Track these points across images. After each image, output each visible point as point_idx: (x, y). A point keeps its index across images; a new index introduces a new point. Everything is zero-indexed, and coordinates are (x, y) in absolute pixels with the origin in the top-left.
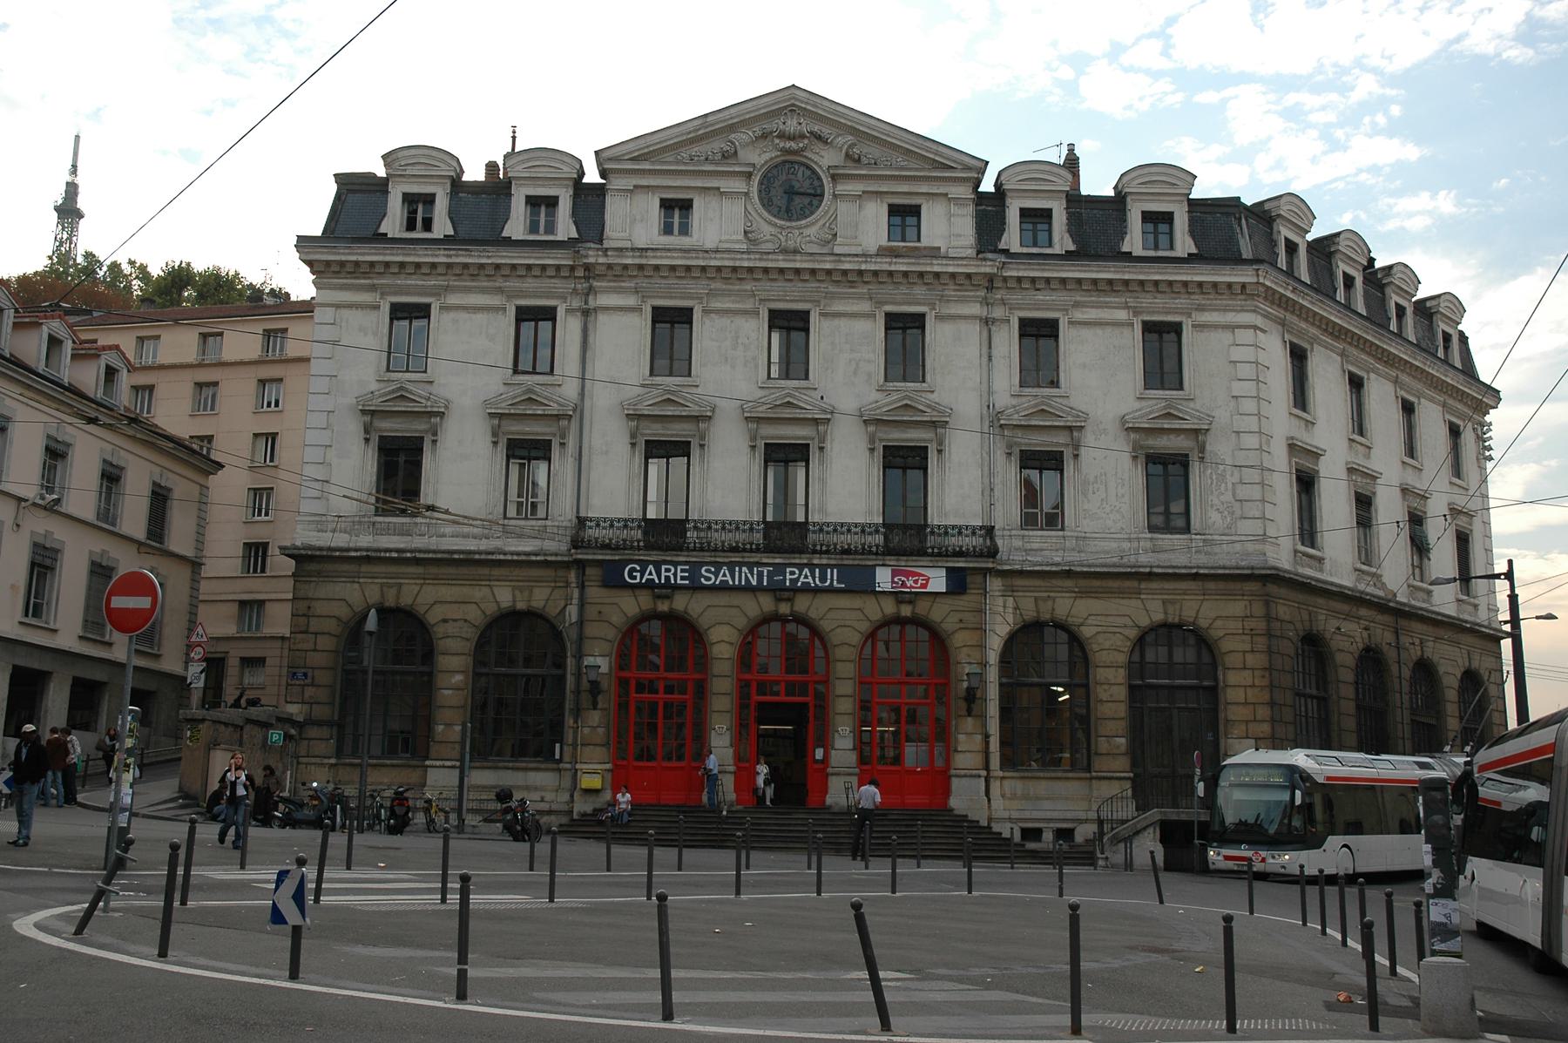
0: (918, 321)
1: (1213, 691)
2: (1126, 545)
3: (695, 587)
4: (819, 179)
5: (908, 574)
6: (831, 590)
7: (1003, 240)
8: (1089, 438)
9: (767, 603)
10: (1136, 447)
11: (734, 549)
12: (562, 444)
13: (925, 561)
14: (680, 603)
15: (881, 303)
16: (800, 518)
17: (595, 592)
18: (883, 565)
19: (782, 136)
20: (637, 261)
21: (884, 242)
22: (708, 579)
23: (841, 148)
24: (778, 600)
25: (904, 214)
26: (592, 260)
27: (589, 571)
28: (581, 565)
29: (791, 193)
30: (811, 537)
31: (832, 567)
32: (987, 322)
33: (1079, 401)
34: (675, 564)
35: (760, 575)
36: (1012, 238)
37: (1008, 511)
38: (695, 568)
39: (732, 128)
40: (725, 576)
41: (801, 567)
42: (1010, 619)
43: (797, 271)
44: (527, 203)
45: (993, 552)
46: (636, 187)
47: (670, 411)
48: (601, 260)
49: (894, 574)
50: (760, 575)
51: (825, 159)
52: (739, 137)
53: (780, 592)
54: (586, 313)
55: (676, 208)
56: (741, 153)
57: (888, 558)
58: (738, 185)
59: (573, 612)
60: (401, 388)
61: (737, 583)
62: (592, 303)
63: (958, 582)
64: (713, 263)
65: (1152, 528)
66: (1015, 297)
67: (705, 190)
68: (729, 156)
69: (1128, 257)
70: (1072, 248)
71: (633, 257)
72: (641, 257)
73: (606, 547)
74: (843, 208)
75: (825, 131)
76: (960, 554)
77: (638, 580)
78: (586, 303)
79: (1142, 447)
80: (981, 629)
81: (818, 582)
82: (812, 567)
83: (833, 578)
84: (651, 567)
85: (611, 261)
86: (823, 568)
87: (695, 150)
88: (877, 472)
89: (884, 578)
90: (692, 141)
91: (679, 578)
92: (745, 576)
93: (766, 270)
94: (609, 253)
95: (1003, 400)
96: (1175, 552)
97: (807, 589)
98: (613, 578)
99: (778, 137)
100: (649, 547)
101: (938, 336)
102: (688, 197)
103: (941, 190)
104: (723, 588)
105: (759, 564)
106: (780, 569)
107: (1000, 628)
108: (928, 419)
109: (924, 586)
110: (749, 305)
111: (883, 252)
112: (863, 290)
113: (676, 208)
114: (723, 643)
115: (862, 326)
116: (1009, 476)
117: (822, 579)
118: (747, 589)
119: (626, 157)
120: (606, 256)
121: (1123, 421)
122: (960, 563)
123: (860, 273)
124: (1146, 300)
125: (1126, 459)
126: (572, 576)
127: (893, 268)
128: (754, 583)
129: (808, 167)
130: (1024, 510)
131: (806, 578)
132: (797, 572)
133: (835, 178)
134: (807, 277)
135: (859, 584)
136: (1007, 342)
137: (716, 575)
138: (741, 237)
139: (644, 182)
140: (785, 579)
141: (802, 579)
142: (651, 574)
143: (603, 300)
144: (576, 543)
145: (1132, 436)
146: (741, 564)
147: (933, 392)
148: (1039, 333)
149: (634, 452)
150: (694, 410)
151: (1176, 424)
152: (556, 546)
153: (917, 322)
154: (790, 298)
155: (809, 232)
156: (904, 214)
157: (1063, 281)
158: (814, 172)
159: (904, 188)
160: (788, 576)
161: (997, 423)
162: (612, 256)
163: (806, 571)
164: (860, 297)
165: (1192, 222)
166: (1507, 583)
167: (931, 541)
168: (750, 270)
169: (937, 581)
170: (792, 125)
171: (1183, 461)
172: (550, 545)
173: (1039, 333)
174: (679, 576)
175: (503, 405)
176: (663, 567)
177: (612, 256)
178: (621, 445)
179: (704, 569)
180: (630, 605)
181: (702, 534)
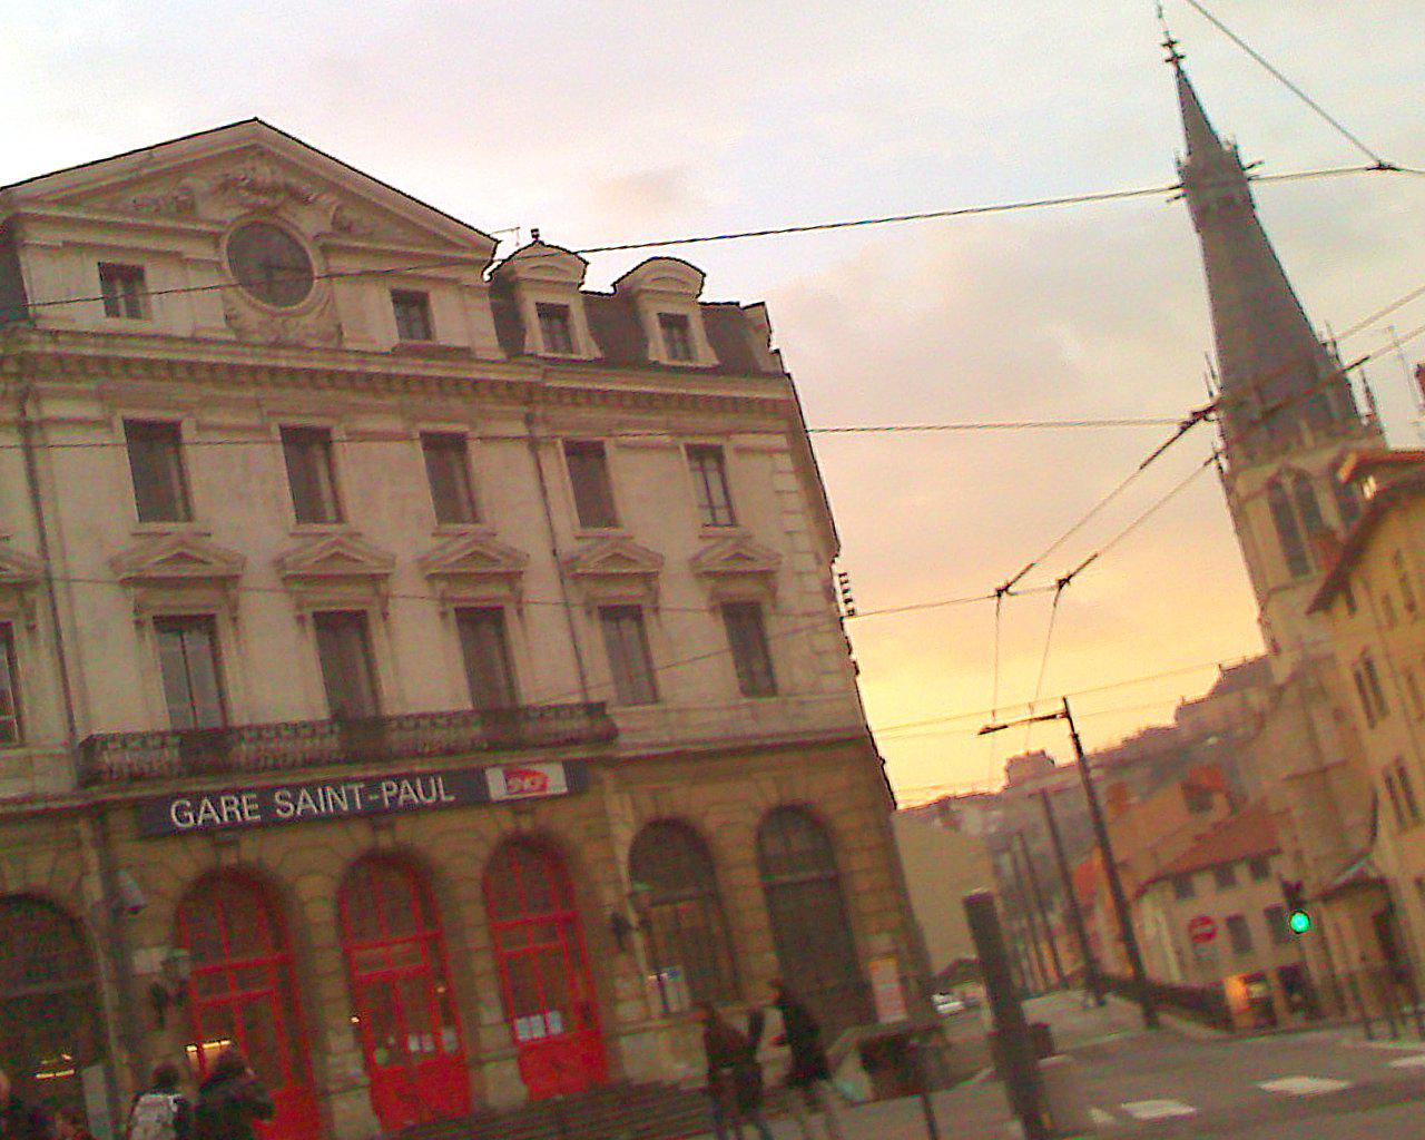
0: (458, 443)
1: (835, 882)
2: (726, 715)
3: (270, 822)
4: (302, 250)
5: (524, 774)
6: (438, 806)
7: (527, 344)
8: (664, 584)
9: (360, 837)
10: (714, 595)
11: (310, 762)
12: (32, 629)
13: (540, 755)
14: (250, 850)
15: (415, 419)
16: (369, 711)
17: (129, 849)
18: (494, 766)
19: (253, 187)
20: (102, 352)
21: (396, 339)
22: (286, 810)
23: (326, 212)
24: (375, 828)
25: (411, 305)
26: (34, 348)
27: (114, 819)
28: (98, 812)
29: (269, 267)
30: (244, 749)
31: (435, 774)
32: (533, 444)
33: (643, 539)
34: (239, 792)
35: (350, 794)
36: (536, 339)
37: (602, 685)
38: (264, 795)
39: (181, 170)
40: (305, 803)
41: (398, 779)
42: (630, 818)
43: (312, 374)
44: (395, 302)
45: (610, 735)
46: (66, 244)
47: (186, 571)
48: (49, 349)
49: (508, 775)
50: (350, 794)
51: (308, 223)
52: (199, 183)
53: (374, 815)
54: (25, 427)
55: (122, 281)
56: (201, 206)
57: (502, 754)
58: (203, 251)
59: (94, 889)
60: (183, 542)
61: (323, 809)
62: (32, 414)
63: (578, 777)
64: (204, 358)
65: (746, 692)
66: (559, 414)
67: (441, 281)
68: (186, 208)
69: (656, 366)
70: (598, 354)
71: (96, 346)
72: (105, 346)
73: (137, 777)
74: (340, 288)
75: (305, 186)
76: (574, 741)
77: (290, 813)
78: (24, 413)
79: (453, 600)
80: (606, 837)
81: (422, 797)
82: (411, 777)
83: (439, 791)
84: (206, 801)
85: (61, 349)
86: (425, 777)
87: (135, 195)
88: (309, 648)
89: (497, 785)
90: (137, 182)
91: (246, 813)
92: (333, 800)
93: (273, 371)
94: (60, 338)
95: (568, 545)
96: (770, 720)
97: (411, 809)
98: (154, 824)
99: (248, 188)
100: (196, 771)
101: (349, 457)
102: (564, 303)
103: (452, 275)
104: (307, 819)
105: (347, 780)
106: (372, 784)
107: (624, 833)
108: (639, 570)
109: (544, 787)
110: (253, 419)
111: (396, 353)
112: (391, 401)
113: (122, 281)
114: (315, 898)
115: (395, 449)
116: (594, 636)
117: (427, 793)
118: (338, 818)
119: (51, 198)
120: (57, 342)
121: (279, 563)
122: (578, 753)
123: (388, 378)
124: (688, 420)
125: (434, 622)
126: (84, 829)
127: (427, 373)
128: (345, 808)
129: (282, 231)
130: (12, 717)
131: (408, 793)
132: (395, 786)
133: (325, 251)
134: (140, 372)
135: (471, 792)
136: (557, 468)
137: (295, 801)
138: (223, 324)
139: (76, 237)
140: (381, 800)
141: (402, 797)
142: (206, 812)
143: (52, 409)
144: (90, 776)
145: (132, 591)
146: (324, 784)
147: (209, 535)
148: (586, 457)
149: (143, 636)
150: (217, 568)
151: (748, 567)
152: (56, 782)
153: (458, 443)
154: (304, 409)
155: (305, 321)
156: (411, 305)
157: (604, 394)
158: (295, 242)
159: (125, 241)
160: (386, 794)
161: (568, 570)
162: (64, 343)
163: (405, 784)
164: (387, 410)
165: (708, 326)
166: (1066, 720)
167: (395, 739)
168: (254, 370)
169: (556, 780)
170: (264, 173)
171: (358, 620)
172: (44, 784)
173: (586, 457)
174: (245, 809)
175: (308, 563)
176: (223, 800)
177: (64, 343)
178: (121, 625)
179: (277, 796)
180: (182, 864)
181: (272, 745)
